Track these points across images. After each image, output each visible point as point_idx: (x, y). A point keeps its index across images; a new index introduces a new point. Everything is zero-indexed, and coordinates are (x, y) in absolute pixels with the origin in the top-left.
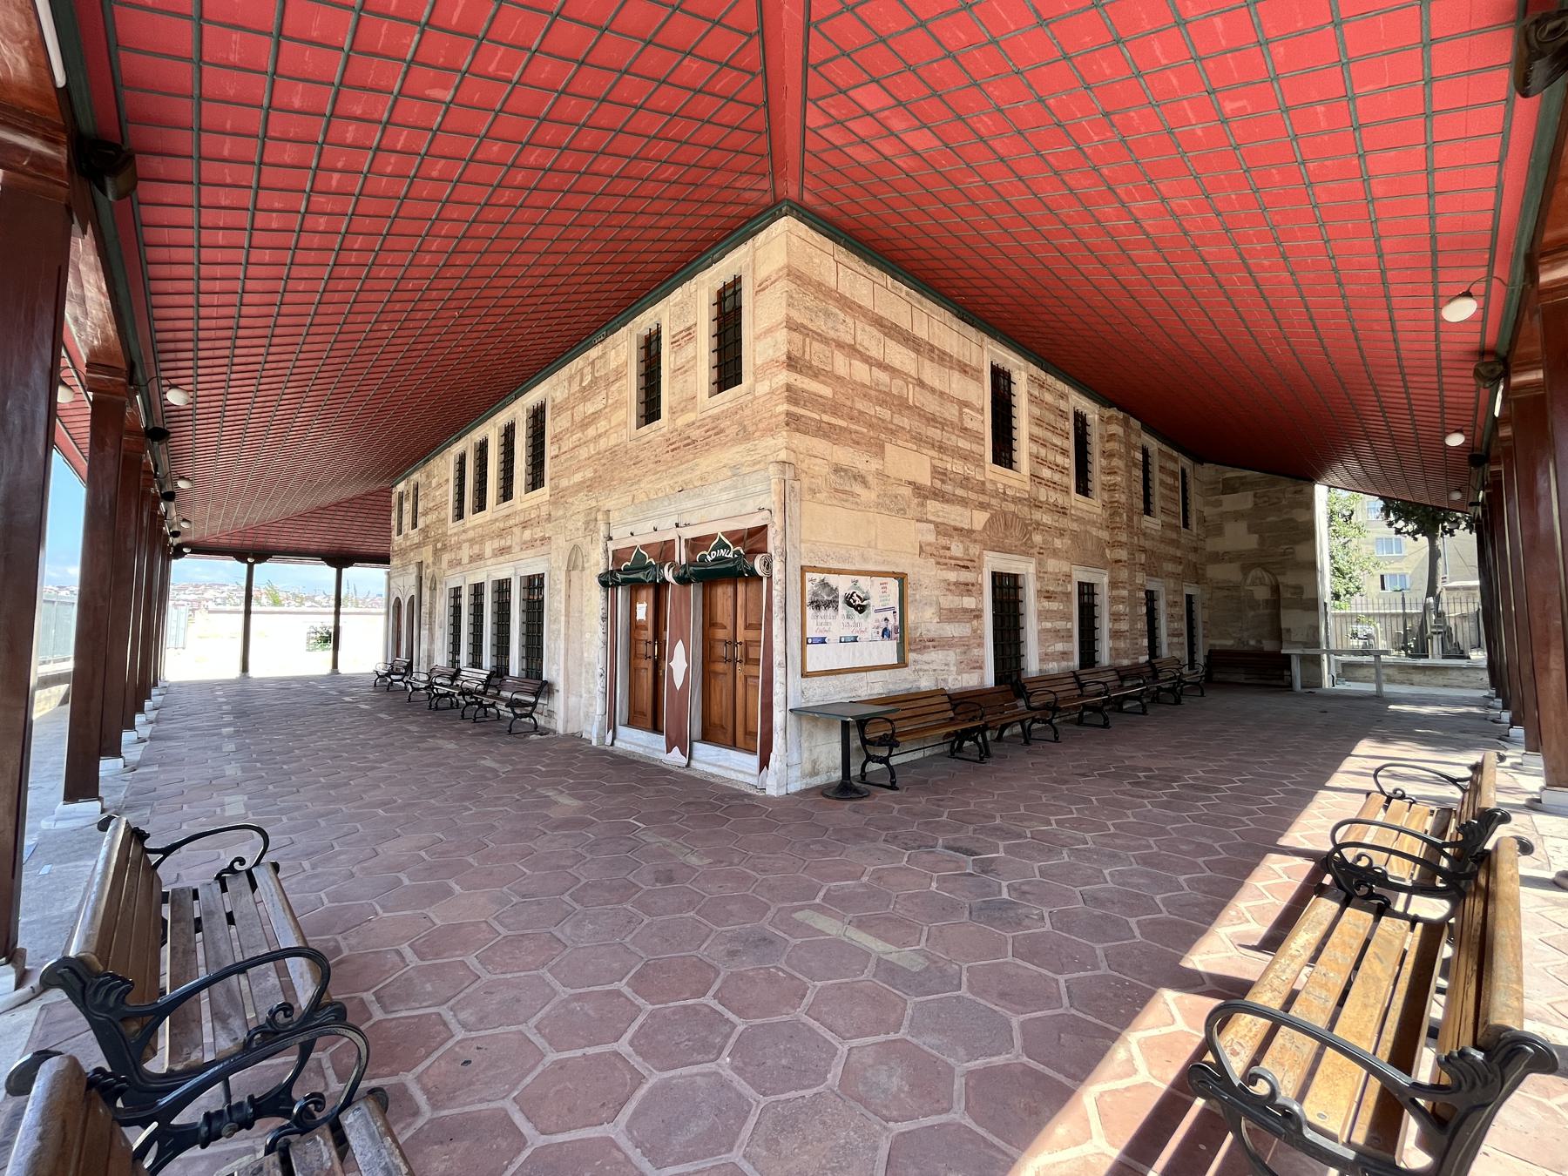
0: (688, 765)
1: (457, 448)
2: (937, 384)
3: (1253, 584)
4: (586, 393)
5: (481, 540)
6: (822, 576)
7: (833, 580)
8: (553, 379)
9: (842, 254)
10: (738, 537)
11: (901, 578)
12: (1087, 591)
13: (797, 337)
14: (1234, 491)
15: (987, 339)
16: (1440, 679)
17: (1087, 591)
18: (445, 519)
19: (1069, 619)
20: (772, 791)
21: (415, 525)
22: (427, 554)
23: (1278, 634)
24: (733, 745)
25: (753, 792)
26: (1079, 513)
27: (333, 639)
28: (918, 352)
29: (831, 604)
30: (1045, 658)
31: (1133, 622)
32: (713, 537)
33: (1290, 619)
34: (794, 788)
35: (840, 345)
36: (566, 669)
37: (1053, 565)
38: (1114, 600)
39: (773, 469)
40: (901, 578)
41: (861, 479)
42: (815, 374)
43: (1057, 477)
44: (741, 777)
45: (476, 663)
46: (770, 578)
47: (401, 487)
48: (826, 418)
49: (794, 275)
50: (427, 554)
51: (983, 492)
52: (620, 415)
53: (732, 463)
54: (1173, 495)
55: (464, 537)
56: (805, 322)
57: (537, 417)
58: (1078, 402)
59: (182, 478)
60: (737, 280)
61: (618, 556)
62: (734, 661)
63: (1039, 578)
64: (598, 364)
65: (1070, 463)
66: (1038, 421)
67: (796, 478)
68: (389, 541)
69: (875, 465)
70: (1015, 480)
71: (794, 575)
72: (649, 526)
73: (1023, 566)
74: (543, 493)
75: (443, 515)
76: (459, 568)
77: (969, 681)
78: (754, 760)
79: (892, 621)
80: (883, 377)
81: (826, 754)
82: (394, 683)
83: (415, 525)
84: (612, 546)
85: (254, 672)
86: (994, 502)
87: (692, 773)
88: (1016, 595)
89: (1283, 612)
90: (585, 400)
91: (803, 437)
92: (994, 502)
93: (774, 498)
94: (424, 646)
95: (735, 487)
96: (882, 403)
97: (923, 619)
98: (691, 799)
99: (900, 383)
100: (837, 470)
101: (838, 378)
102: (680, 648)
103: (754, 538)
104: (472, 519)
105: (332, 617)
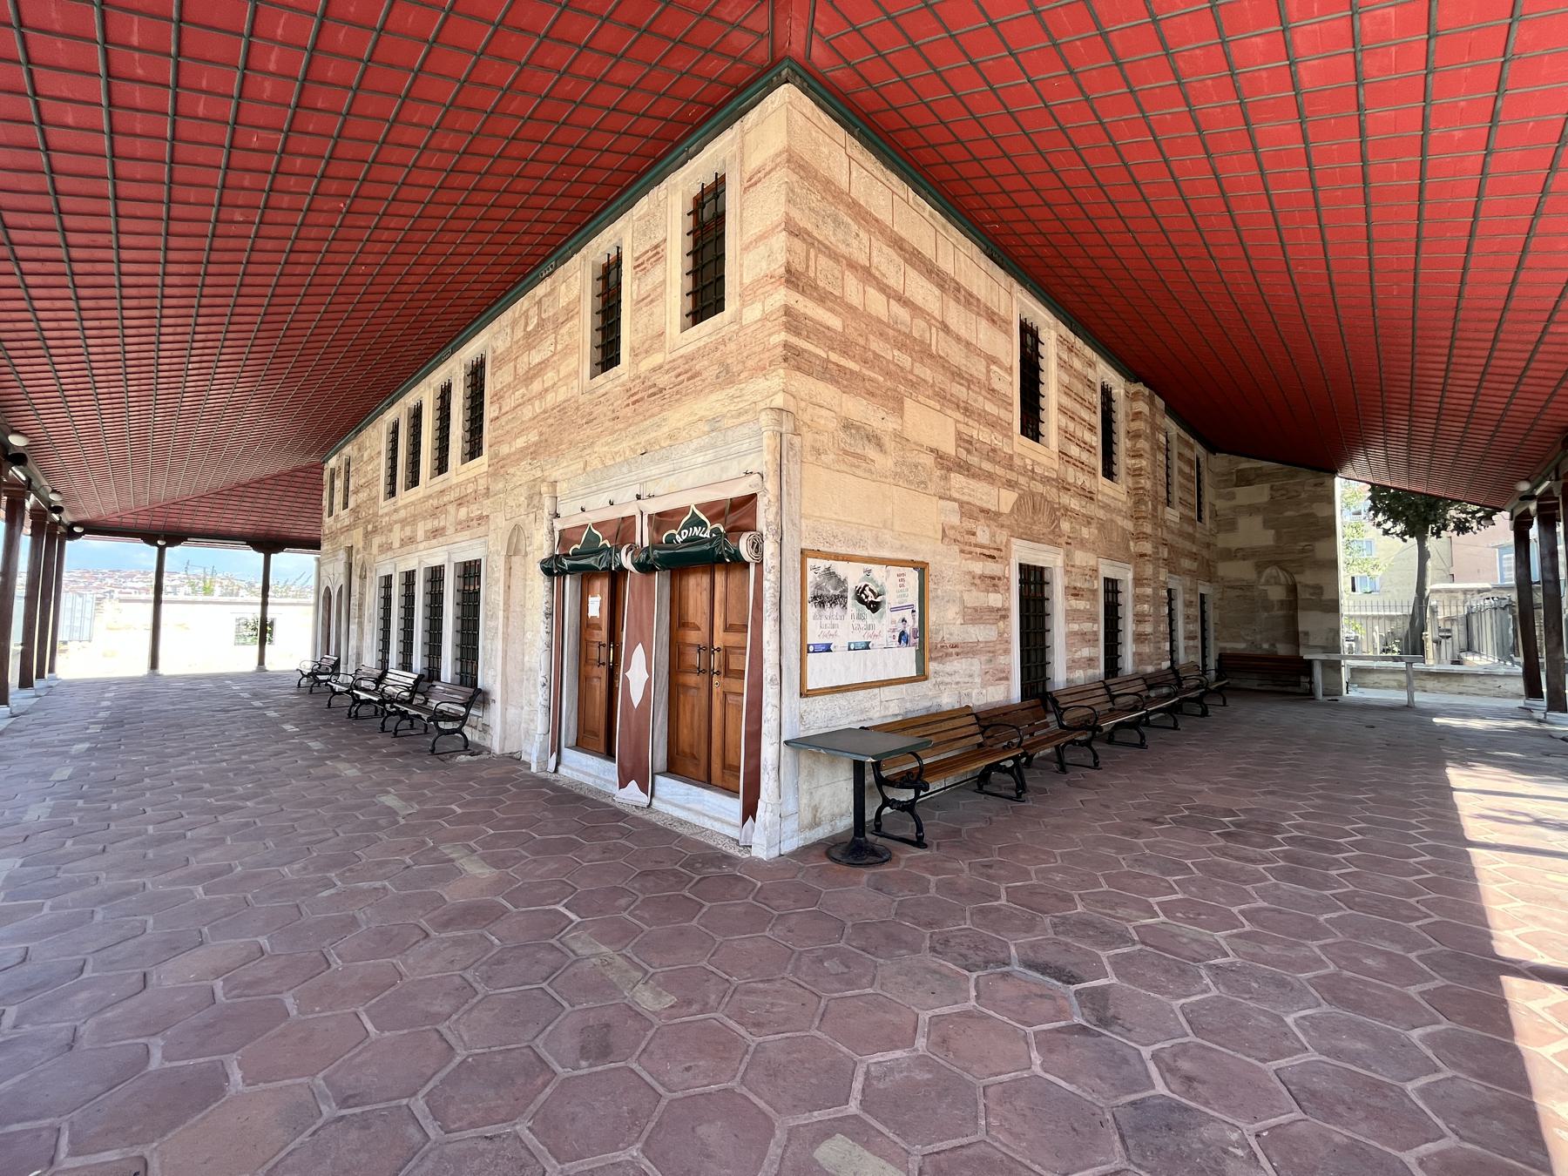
0: (650, 805)
1: (390, 415)
2: (963, 333)
3: (1267, 583)
4: (531, 340)
5: (412, 521)
6: (827, 563)
7: (840, 568)
8: (494, 326)
9: (856, 148)
10: (718, 511)
11: (922, 568)
12: (1112, 587)
13: (798, 245)
14: (1249, 483)
15: (1017, 287)
16: (1455, 686)
17: (1112, 587)
20: (762, 851)
21: (346, 505)
22: (357, 538)
23: (1294, 637)
24: (707, 782)
25: (734, 851)
26: (1105, 499)
27: (264, 630)
28: (941, 287)
29: (838, 600)
31: (1157, 624)
32: (683, 511)
33: (1308, 622)
34: (790, 845)
35: (852, 265)
36: (504, 674)
37: (1082, 558)
38: (1138, 599)
39: (766, 419)
40: (922, 568)
42: (823, 298)
43: (1085, 456)
44: (717, 827)
45: (406, 666)
46: (760, 564)
47: (333, 462)
48: (834, 357)
49: (794, 161)
50: (357, 538)
51: (1011, 468)
52: (572, 362)
53: (710, 414)
54: (1189, 485)
55: (395, 517)
56: (810, 227)
57: (476, 374)
58: (1105, 373)
59: (17, 432)
60: (720, 182)
61: (565, 538)
62: (709, 672)
64: (546, 302)
65: (1096, 440)
66: (1067, 390)
67: (796, 432)
68: (320, 524)
69: (892, 424)
70: (1043, 455)
71: (792, 562)
72: (603, 499)
73: (1047, 557)
74: (481, 463)
75: (374, 493)
76: (390, 554)
78: (735, 806)
80: (903, 313)
81: (830, 799)
82: (317, 681)
83: (346, 505)
85: (165, 668)
86: (1022, 480)
87: (653, 818)
88: (1042, 592)
89: (1300, 614)
90: (529, 347)
91: (804, 378)
92: (1022, 480)
93: (767, 457)
94: (353, 643)
95: (713, 446)
96: (902, 347)
97: (946, 621)
98: (649, 866)
99: (923, 324)
100: (848, 425)
102: (639, 654)
104: (405, 496)
105: (259, 608)
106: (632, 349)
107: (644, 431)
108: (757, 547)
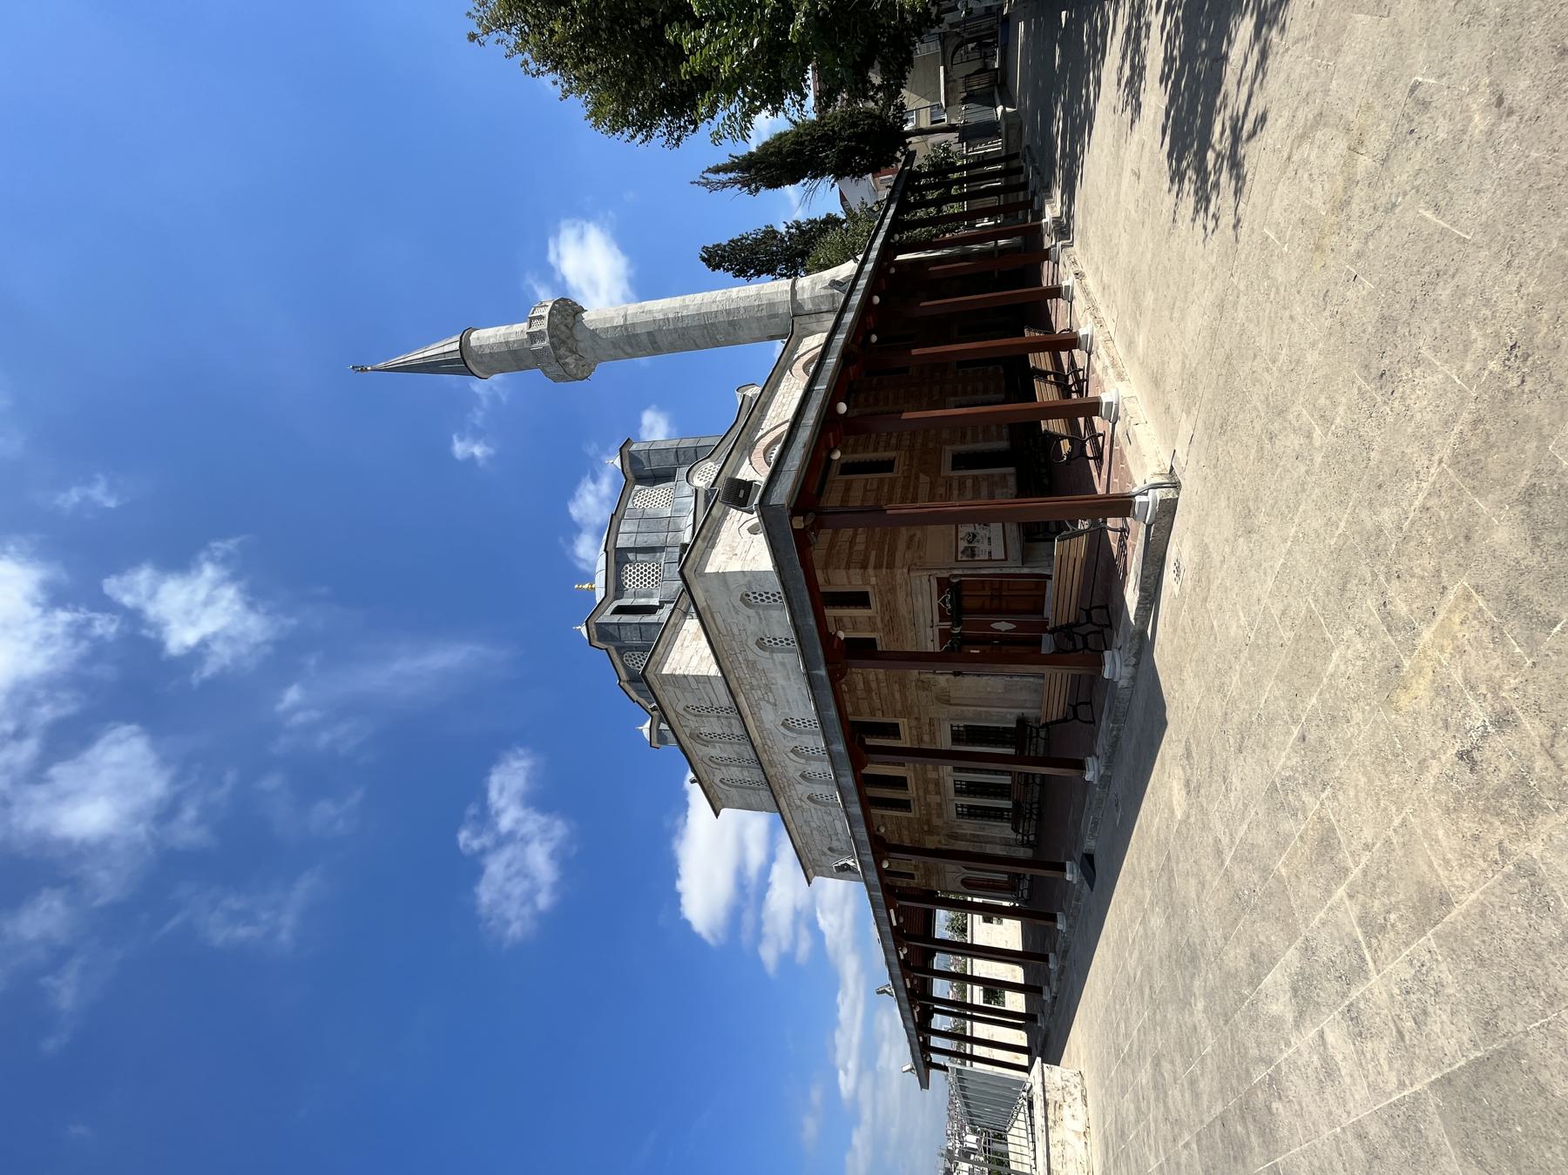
7: (961, 549)
18: (910, 820)
29: (973, 549)
30: (1000, 438)
41: (911, 538)
73: (948, 452)
74: (903, 723)
77: (1012, 481)
102: (995, 626)
103: (943, 584)
108: (955, 576)
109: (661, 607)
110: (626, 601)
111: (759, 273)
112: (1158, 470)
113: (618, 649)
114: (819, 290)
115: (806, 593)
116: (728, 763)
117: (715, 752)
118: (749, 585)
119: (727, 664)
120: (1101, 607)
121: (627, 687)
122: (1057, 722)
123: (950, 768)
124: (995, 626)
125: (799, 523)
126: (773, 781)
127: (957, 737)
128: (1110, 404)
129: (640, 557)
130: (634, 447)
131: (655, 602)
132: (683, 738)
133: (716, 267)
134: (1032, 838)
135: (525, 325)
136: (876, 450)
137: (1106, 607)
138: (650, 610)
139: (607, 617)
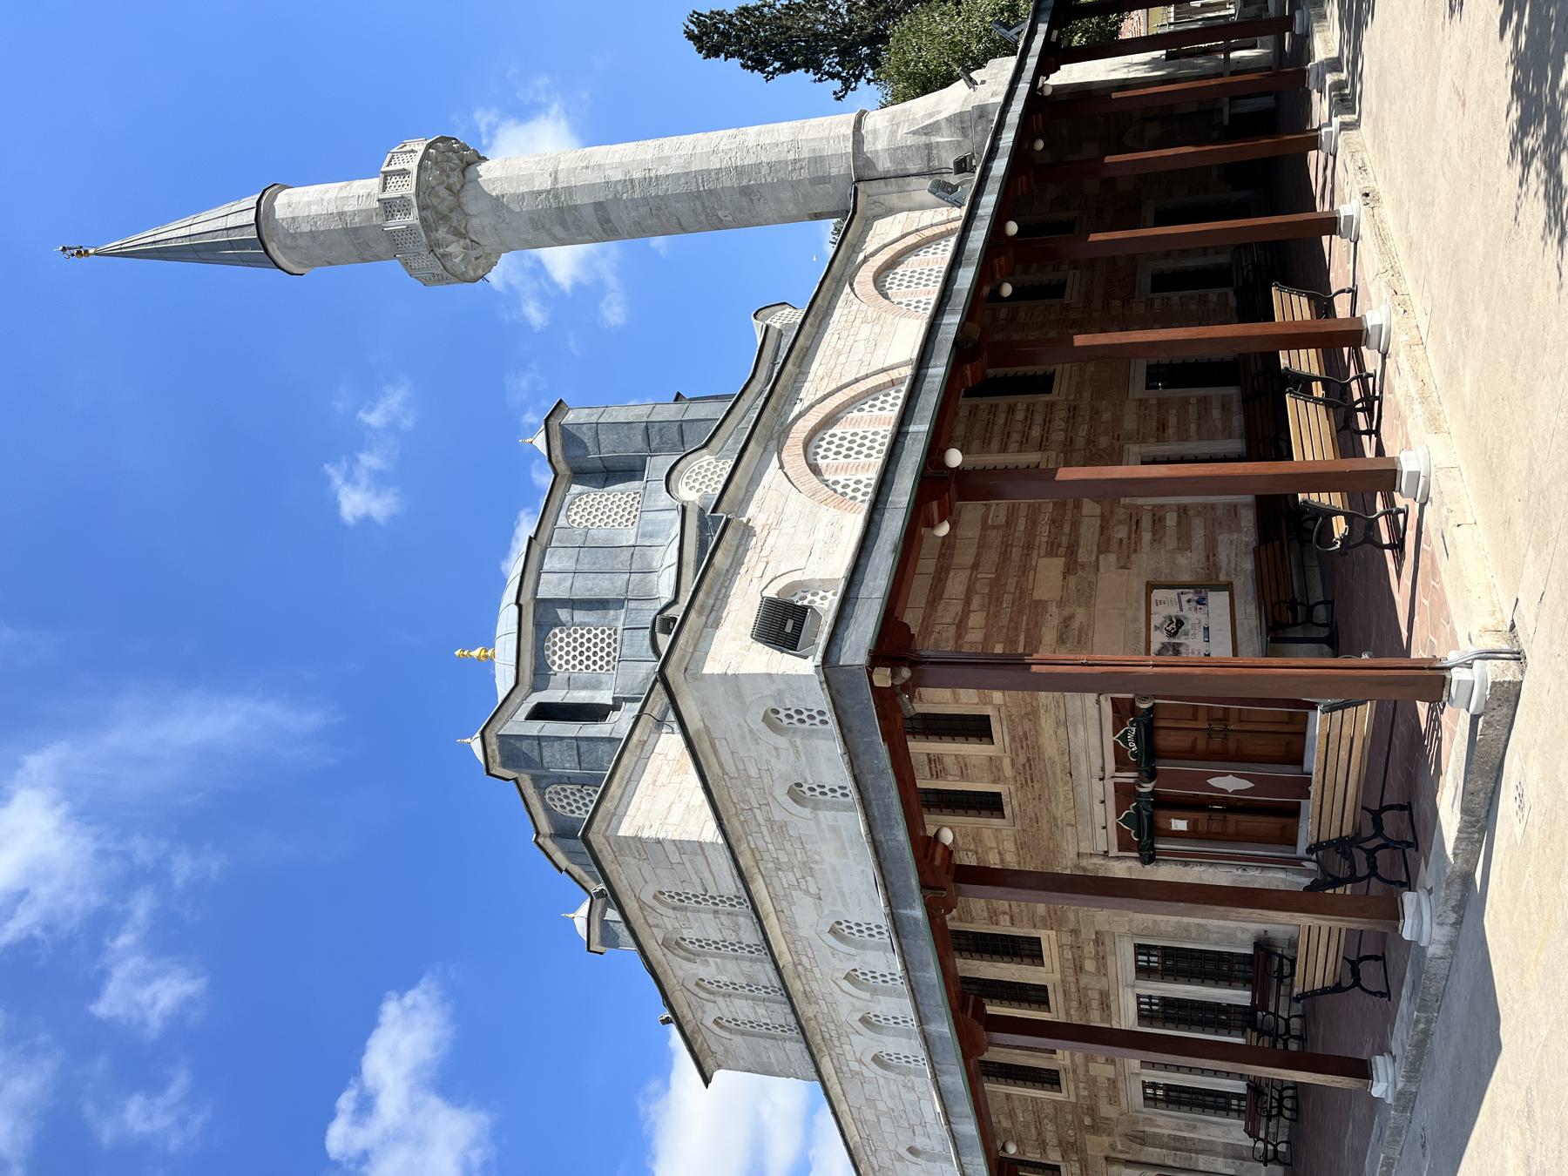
2: (973, 551)
10: (1118, 723)
11: (1151, 587)
19: (1186, 401)
28: (948, 570)
32: (1116, 743)
37: (1130, 423)
41: (1067, 621)
55: (1081, 1072)
63: (1143, 440)
69: (1053, 609)
75: (1049, 1110)
79: (1190, 596)
80: (976, 602)
84: (1114, 852)
101: (986, 637)
102: (1214, 782)
106: (994, 782)
107: (1054, 774)
109: (616, 707)
110: (554, 695)
111: (789, 67)
112: (1490, 623)
113: (535, 780)
114: (903, 136)
115: (894, 794)
116: (729, 991)
117: (707, 971)
118: (780, 695)
119: (734, 826)
120: (1401, 808)
121: (549, 845)
122: (1324, 991)
123: (1135, 1063)
124: (1214, 782)
125: (883, 678)
126: (811, 1027)
127: (1143, 1017)
128: (1415, 476)
129: (579, 616)
130: (570, 418)
131: (604, 697)
132: (653, 948)
133: (713, 52)
134: (1282, 1148)
135: (376, 182)
136: (1004, 449)
137: (1407, 807)
138: (595, 713)
139: (517, 724)
